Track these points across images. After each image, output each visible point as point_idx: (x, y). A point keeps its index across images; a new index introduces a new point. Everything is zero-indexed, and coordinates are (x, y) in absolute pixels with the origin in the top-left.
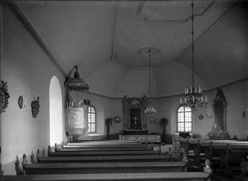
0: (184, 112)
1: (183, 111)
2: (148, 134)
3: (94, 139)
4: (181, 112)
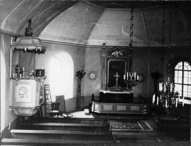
0: (183, 70)
1: (182, 69)
2: (134, 102)
3: (31, 115)
4: (178, 70)
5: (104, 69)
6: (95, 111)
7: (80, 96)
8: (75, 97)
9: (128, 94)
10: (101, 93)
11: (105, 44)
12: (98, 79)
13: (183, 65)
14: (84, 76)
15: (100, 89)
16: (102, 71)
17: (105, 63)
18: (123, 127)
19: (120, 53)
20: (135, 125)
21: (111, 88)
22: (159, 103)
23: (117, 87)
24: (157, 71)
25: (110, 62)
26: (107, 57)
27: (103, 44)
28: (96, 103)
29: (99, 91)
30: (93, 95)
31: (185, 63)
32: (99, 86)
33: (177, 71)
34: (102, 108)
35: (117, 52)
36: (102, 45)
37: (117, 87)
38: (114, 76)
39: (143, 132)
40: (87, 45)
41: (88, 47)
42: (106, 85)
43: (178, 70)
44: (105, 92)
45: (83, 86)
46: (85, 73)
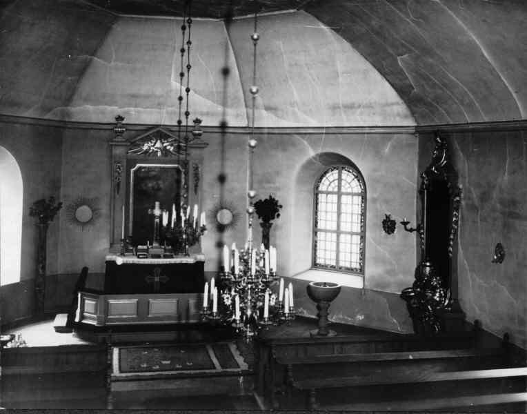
0: (339, 194)
4: (328, 193)
5: (118, 193)
6: (84, 321)
7: (44, 276)
8: (27, 278)
9: (186, 265)
10: (111, 264)
11: (122, 119)
12: (103, 223)
13: (340, 179)
14: (56, 214)
15: (108, 250)
16: (113, 198)
17: (123, 174)
18: (161, 365)
19: (165, 145)
20: (200, 357)
21: (140, 247)
22: (218, 308)
24: (270, 197)
25: (135, 172)
28: (88, 296)
29: (104, 258)
30: (85, 270)
31: (345, 174)
32: (104, 244)
33: (324, 195)
34: (106, 309)
35: (157, 141)
36: (113, 121)
39: (219, 375)
41: (70, 128)
42: (124, 241)
43: (328, 193)
45: (56, 245)
46: (60, 204)
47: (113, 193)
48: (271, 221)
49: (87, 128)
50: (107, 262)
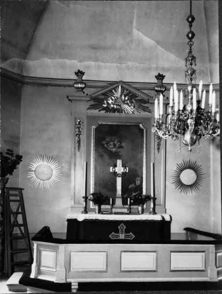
2: (172, 238)
5: (79, 149)
6: (41, 277)
11: (83, 74)
23: (119, 202)
26: (89, 114)
27: (76, 74)
37: (119, 202)
38: (111, 171)
40: (25, 74)
44: (81, 217)
47: (73, 150)
48: (8, 176)
49: (44, 84)
50: (68, 220)
